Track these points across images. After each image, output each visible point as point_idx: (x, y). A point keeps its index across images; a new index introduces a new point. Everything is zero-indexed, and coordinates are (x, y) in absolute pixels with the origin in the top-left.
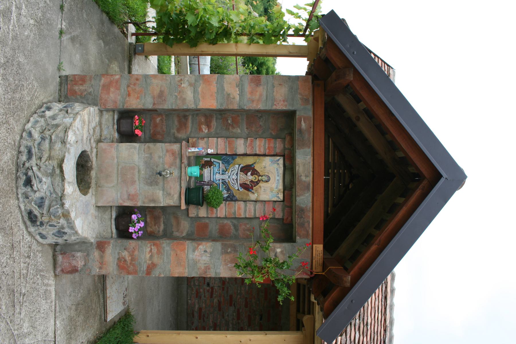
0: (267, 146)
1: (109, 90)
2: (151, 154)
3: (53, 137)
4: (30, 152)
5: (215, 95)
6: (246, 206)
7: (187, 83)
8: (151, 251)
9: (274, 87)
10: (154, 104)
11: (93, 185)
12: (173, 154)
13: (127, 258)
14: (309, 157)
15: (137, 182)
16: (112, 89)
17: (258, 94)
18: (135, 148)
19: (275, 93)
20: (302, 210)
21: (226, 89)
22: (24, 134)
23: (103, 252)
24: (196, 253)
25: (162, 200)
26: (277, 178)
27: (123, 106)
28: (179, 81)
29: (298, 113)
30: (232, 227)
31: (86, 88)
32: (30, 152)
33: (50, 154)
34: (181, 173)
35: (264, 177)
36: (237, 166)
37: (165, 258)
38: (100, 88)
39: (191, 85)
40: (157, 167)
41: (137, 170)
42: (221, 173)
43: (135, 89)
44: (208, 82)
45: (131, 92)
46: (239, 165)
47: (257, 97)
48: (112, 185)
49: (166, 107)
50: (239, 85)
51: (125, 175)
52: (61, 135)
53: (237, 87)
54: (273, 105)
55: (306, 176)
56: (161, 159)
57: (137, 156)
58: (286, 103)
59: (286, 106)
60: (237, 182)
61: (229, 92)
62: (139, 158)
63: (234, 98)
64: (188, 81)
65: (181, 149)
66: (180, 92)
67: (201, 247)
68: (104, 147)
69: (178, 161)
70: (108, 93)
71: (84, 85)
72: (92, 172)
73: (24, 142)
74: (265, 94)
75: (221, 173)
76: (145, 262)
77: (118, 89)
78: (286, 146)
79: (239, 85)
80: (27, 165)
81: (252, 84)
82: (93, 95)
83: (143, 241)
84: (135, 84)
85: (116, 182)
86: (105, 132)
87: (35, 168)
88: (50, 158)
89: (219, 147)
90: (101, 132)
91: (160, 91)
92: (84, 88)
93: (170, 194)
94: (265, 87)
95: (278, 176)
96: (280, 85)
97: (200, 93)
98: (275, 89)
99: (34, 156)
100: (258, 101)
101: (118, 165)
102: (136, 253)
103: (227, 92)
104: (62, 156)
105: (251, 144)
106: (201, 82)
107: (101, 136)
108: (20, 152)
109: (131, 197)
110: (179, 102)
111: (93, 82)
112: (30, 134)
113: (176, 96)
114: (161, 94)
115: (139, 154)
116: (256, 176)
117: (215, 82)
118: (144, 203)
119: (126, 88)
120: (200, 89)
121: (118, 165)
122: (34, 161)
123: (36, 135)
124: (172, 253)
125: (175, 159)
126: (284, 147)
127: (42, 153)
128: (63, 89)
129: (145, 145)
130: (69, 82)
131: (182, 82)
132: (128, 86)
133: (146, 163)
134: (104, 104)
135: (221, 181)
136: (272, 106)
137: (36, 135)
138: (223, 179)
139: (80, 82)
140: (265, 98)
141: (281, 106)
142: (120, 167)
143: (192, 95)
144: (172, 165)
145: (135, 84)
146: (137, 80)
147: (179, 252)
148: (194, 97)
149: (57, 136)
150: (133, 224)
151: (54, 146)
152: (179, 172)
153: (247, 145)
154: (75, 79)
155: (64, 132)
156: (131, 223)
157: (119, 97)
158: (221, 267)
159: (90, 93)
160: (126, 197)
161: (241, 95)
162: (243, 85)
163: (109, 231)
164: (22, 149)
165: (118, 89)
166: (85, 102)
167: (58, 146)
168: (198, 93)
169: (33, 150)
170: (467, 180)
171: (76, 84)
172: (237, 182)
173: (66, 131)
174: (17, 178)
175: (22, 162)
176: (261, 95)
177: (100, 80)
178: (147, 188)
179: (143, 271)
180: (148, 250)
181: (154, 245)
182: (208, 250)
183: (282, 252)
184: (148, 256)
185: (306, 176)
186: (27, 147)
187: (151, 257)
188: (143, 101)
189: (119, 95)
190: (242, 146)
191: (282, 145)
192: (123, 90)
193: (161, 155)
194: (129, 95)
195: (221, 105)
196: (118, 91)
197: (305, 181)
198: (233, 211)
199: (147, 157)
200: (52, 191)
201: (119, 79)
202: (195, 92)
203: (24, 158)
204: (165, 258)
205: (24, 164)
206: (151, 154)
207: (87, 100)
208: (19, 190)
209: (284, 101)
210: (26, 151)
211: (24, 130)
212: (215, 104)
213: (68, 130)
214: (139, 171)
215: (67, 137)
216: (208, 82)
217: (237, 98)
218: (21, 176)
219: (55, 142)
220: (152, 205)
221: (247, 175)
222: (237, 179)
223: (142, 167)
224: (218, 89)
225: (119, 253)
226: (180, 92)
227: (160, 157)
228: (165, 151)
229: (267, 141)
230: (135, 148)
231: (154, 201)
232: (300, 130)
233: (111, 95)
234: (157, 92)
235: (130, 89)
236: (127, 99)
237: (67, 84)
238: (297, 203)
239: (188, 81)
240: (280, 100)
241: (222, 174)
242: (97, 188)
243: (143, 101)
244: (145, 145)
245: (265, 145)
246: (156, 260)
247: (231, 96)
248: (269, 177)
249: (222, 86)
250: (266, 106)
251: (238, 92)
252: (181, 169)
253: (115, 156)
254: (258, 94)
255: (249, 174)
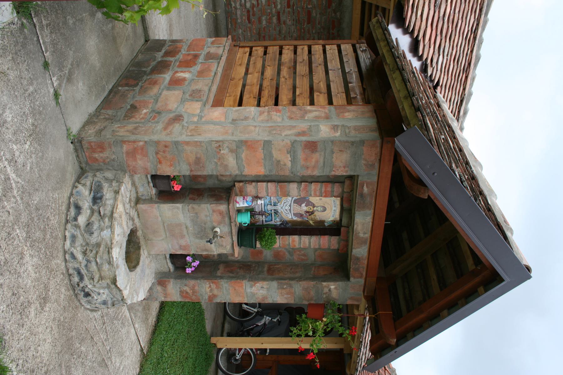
0: (323, 190)
1: (135, 157)
2: (196, 213)
3: (98, 260)
4: (79, 273)
5: (263, 161)
6: (300, 239)
7: (227, 149)
8: (210, 287)
9: (332, 152)
10: (191, 171)
11: (142, 242)
12: (221, 213)
13: (189, 291)
14: (369, 218)
15: (187, 236)
16: (138, 157)
17: (314, 160)
18: (178, 208)
19: (334, 160)
20: (358, 259)
21: (275, 156)
22: (67, 256)
23: (165, 287)
24: (253, 288)
25: (215, 250)
26: (334, 208)
27: (156, 172)
28: (217, 148)
29: (360, 178)
30: (287, 253)
31: (108, 155)
32: (79, 273)
33: (100, 275)
34: (231, 228)
35: (319, 208)
36: (290, 198)
37: (225, 291)
38: (124, 156)
39: (231, 151)
40: (205, 224)
41: (184, 227)
42: (273, 205)
43: (166, 157)
44: (253, 148)
45: (162, 159)
46: (293, 198)
47: (313, 164)
48: (161, 238)
49: (205, 173)
50: (290, 152)
51: (173, 230)
52: (106, 256)
53: (288, 153)
54: (331, 171)
55: (365, 233)
56: (209, 218)
57: (182, 216)
58: (346, 169)
59: (347, 171)
60: (291, 212)
61: (279, 159)
62: (184, 217)
63: (285, 165)
64: (227, 147)
65: (229, 211)
66: (219, 159)
67: (258, 284)
68: (144, 208)
69: (227, 219)
70: (135, 160)
71: (105, 153)
72: (138, 233)
73: (70, 265)
74: (322, 160)
75: (273, 205)
76: (206, 293)
77: (146, 155)
78: (345, 190)
79: (290, 152)
80: (81, 285)
81: (307, 151)
82: (118, 162)
83: (202, 281)
84: (164, 152)
85: (164, 236)
86: (141, 190)
87: (90, 286)
88: (101, 278)
89: (270, 191)
90: (136, 189)
91: (196, 158)
92: (105, 155)
93: (222, 246)
94: (323, 153)
95: (335, 207)
96: (341, 151)
97: (244, 159)
98: (334, 155)
99: (85, 276)
100: (314, 167)
101: (164, 223)
102: (196, 288)
103: (276, 159)
104: (113, 275)
105: (305, 189)
106: (244, 148)
107: (137, 193)
108: (70, 275)
109: (181, 247)
110: (219, 168)
111: (114, 149)
112: (73, 257)
113: (216, 163)
114: (198, 161)
115: (183, 213)
116: (311, 207)
117: (260, 149)
118: (197, 252)
119: (154, 155)
120: (243, 156)
121: (164, 223)
122: (86, 281)
123: (80, 257)
124: (231, 288)
125: (223, 217)
126: (343, 191)
127: (92, 274)
128: (80, 155)
129: (188, 206)
130: (85, 150)
131: (221, 148)
132: (157, 153)
133: (192, 221)
134: (133, 171)
135: (273, 211)
136: (330, 172)
137: (80, 257)
138: (275, 210)
139: (99, 150)
140: (322, 164)
141: (341, 172)
142: (165, 225)
143: (235, 161)
144: (221, 223)
145: (164, 152)
146: (166, 146)
147: (237, 288)
148: (237, 163)
149: (101, 258)
150: (189, 264)
151: (102, 268)
152: (229, 228)
153: (301, 189)
154: (92, 147)
155: (107, 253)
156: (187, 265)
157: (149, 164)
158: (278, 297)
159: (114, 160)
160: (177, 247)
161: (294, 161)
162: (294, 152)
163: (166, 266)
164: (71, 271)
165: (146, 155)
166: (111, 168)
167: (106, 267)
168: (242, 160)
169: (82, 271)
170: (528, 282)
171: (94, 152)
172: (291, 212)
173: (109, 252)
174: (76, 295)
175: (76, 283)
176: (317, 162)
177: (122, 147)
178: (197, 241)
179: (205, 299)
180: (208, 286)
181: (212, 283)
182: (265, 287)
183: (335, 288)
184: (208, 290)
185: (365, 233)
186: (75, 269)
187: (211, 291)
188: (178, 168)
189: (148, 162)
190: (296, 189)
191: (340, 190)
192: (151, 157)
193: (208, 214)
194: (160, 162)
195: (270, 171)
196: (146, 158)
197: (363, 238)
198: (287, 243)
199: (192, 216)
200: (112, 297)
201: (144, 145)
202: (237, 158)
203: (76, 279)
204: (225, 291)
205: (78, 285)
206: (196, 213)
207: (112, 166)
208: (82, 301)
209: (344, 167)
210: (76, 273)
211: (65, 252)
212: (263, 170)
213: (110, 250)
214: (187, 227)
215: (113, 259)
216: (253, 148)
217: (289, 164)
218: (79, 292)
219: (102, 264)
220: (205, 253)
221: (300, 206)
222: (290, 210)
223: (189, 224)
224: (265, 155)
225: (180, 288)
226: (219, 159)
227: (206, 216)
228: (211, 211)
229: (323, 186)
230: (178, 208)
231: (206, 250)
232: (362, 195)
233: (140, 162)
234: (192, 158)
235: (159, 156)
236: (159, 166)
237: (84, 152)
238: (353, 254)
239: (227, 147)
240: (340, 167)
241: (274, 205)
242: (146, 241)
243: (178, 168)
244: (188, 206)
245: (321, 189)
246: (216, 292)
247: (282, 163)
248: (324, 207)
249: (271, 154)
250: (323, 172)
251: (290, 159)
252: (231, 226)
253: (158, 215)
254: (314, 160)
255: (303, 205)
